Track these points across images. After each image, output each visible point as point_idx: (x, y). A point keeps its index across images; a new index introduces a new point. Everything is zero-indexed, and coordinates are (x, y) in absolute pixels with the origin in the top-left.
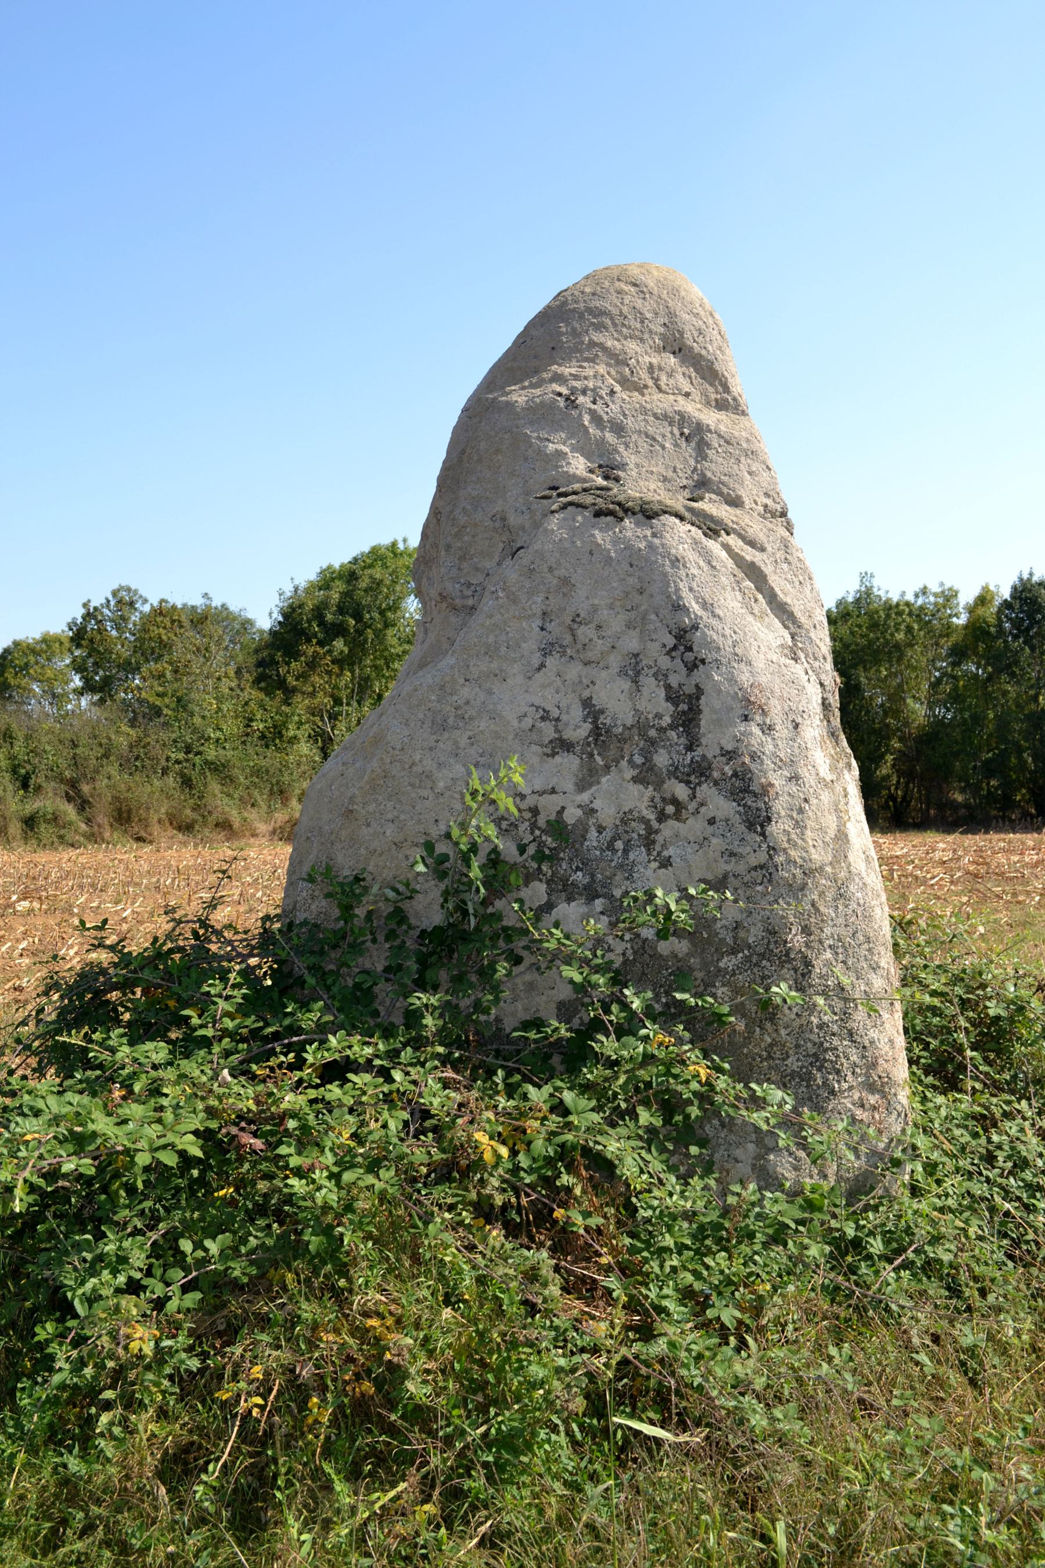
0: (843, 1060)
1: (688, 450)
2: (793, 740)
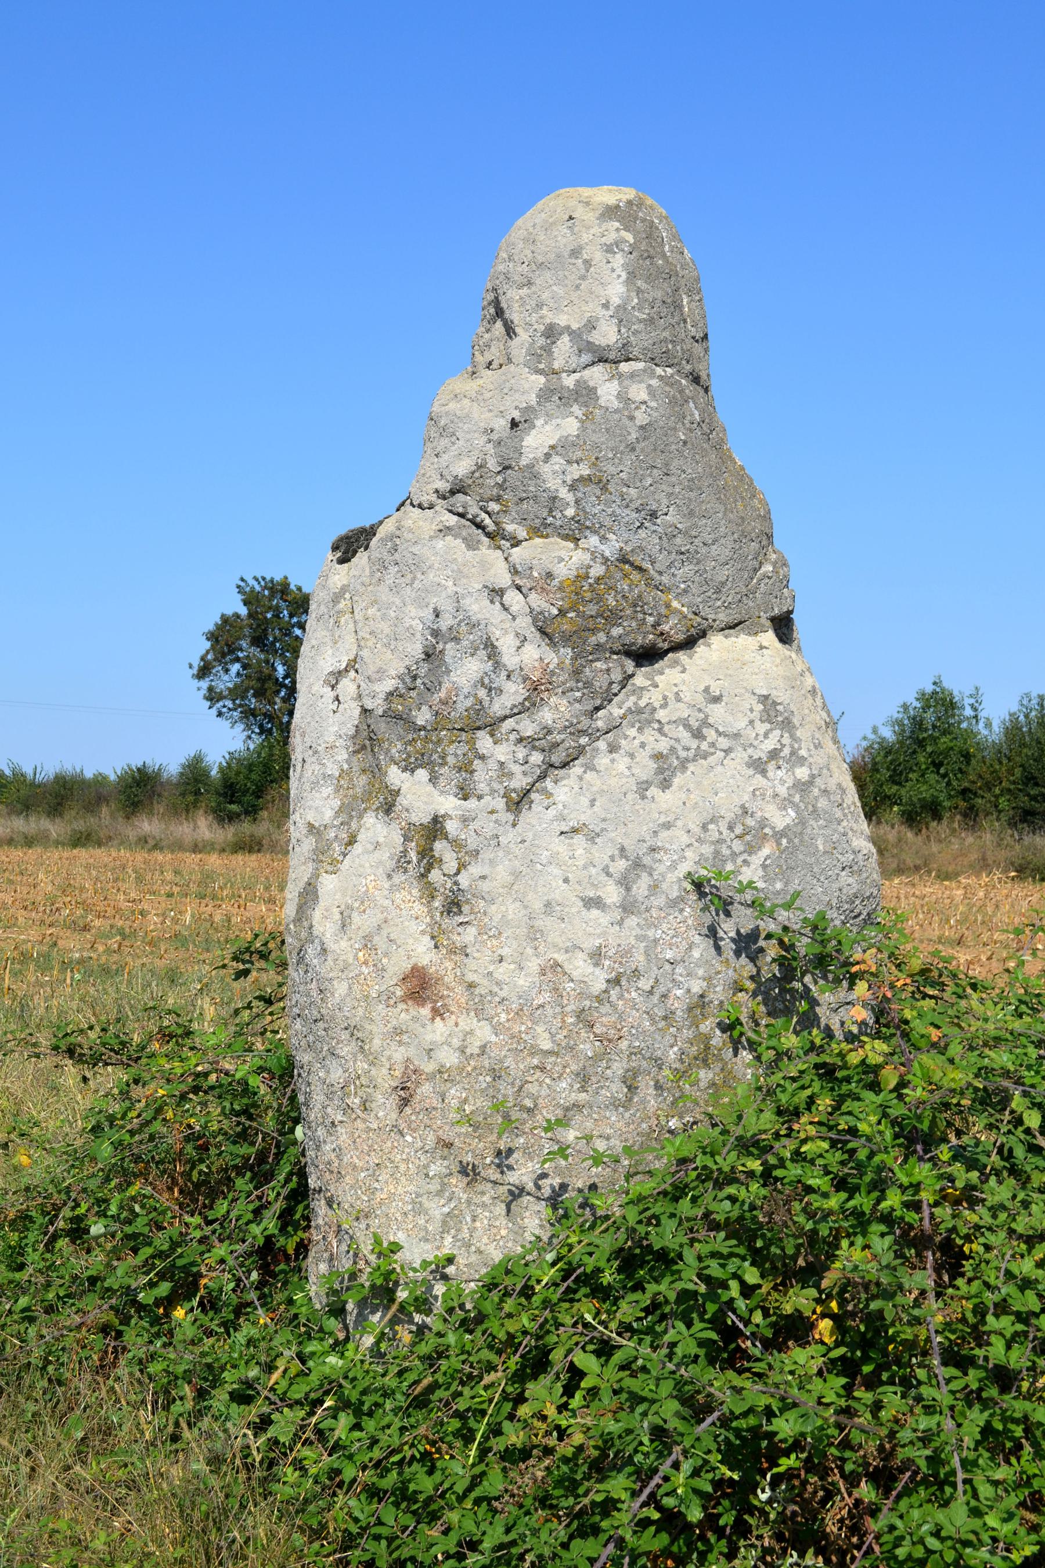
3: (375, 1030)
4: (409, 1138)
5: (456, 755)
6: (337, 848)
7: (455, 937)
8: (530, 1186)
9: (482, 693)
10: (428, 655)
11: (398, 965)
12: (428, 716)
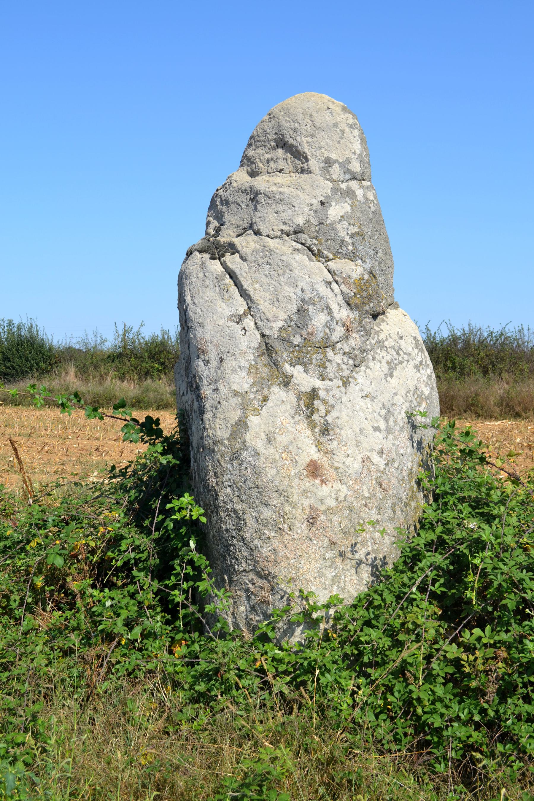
2: (219, 368)
3: (294, 491)
4: (315, 542)
5: (316, 359)
7: (327, 446)
8: (364, 559)
9: (327, 330)
10: (298, 311)
11: (303, 461)
12: (299, 340)
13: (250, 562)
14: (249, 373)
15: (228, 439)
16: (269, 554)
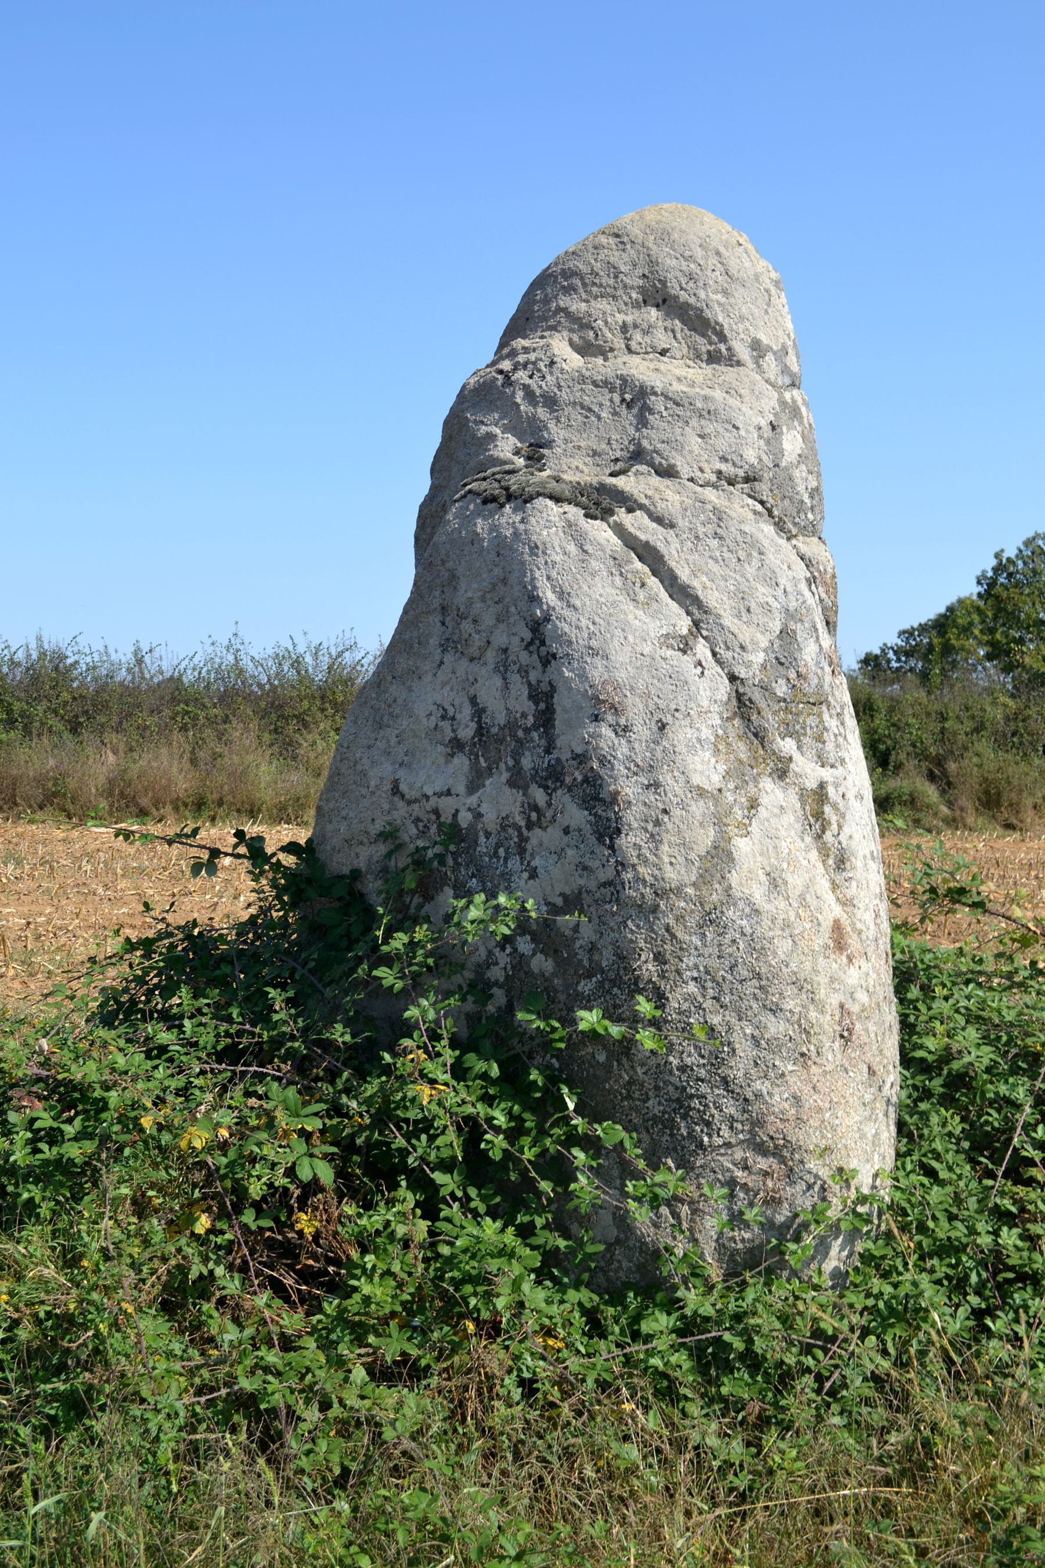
0: (714, 1111)
1: (629, 418)
4: (851, 1074)
6: (739, 813)
12: (784, 688)
13: (740, 1126)
14: (717, 751)
15: (694, 884)
16: (786, 1105)
